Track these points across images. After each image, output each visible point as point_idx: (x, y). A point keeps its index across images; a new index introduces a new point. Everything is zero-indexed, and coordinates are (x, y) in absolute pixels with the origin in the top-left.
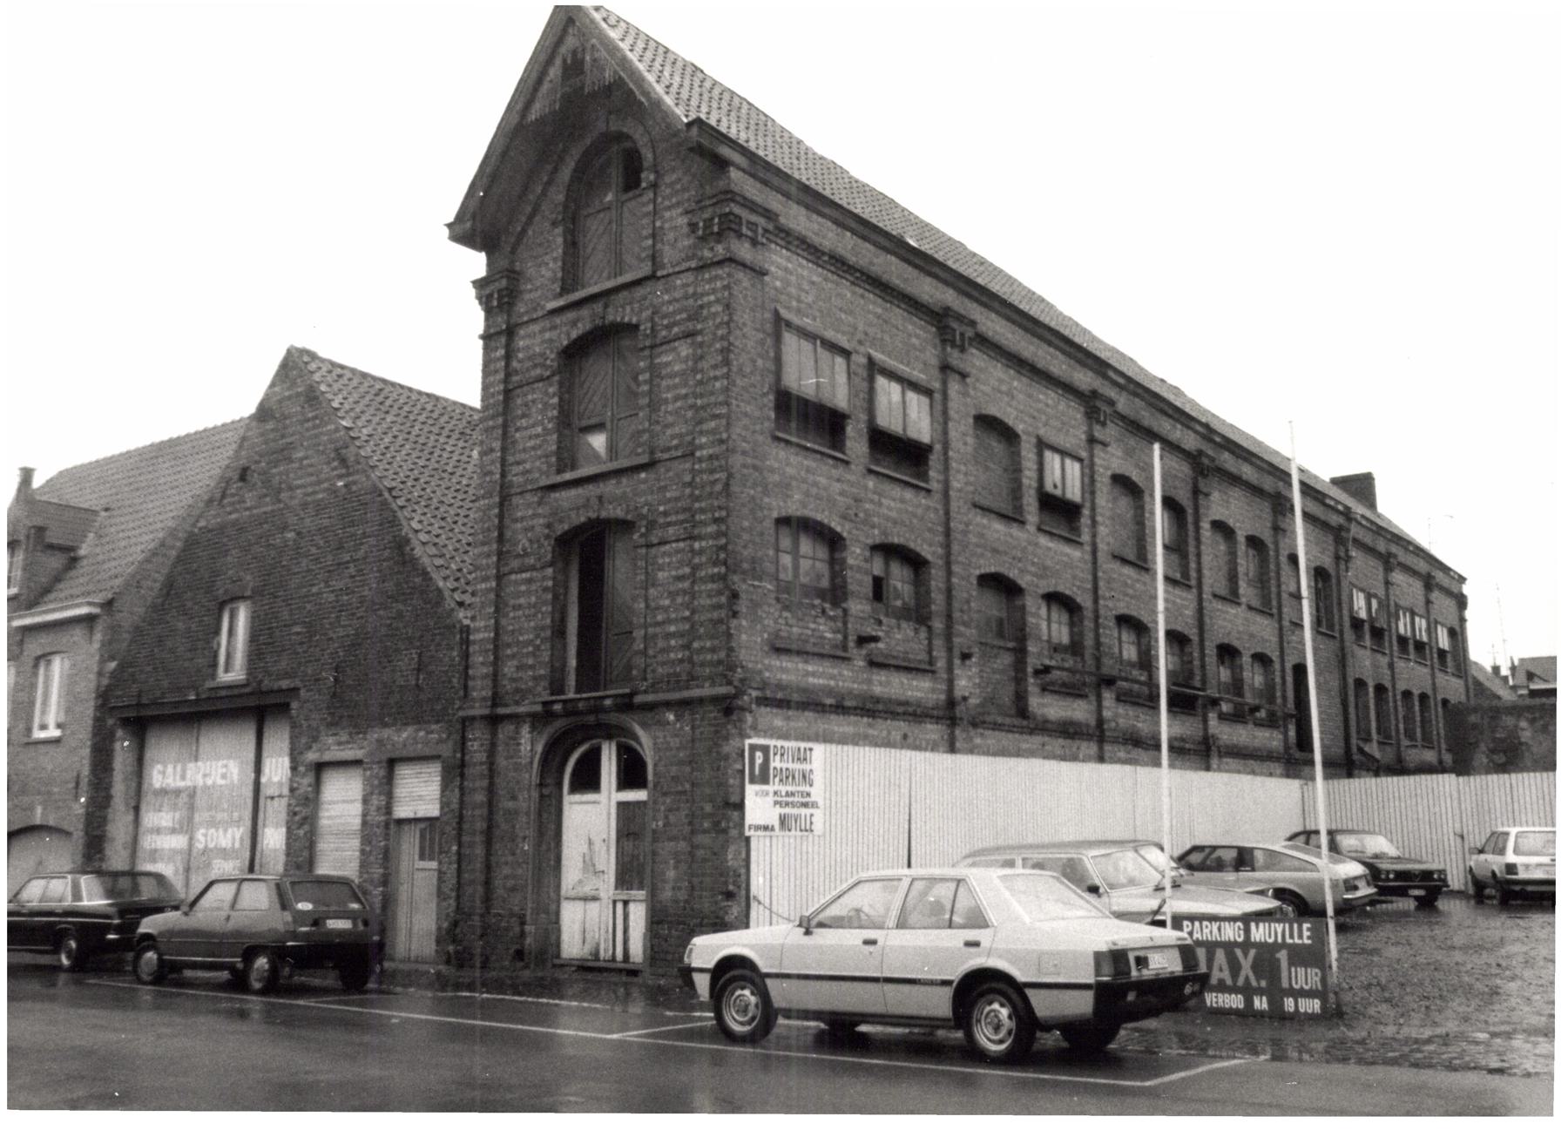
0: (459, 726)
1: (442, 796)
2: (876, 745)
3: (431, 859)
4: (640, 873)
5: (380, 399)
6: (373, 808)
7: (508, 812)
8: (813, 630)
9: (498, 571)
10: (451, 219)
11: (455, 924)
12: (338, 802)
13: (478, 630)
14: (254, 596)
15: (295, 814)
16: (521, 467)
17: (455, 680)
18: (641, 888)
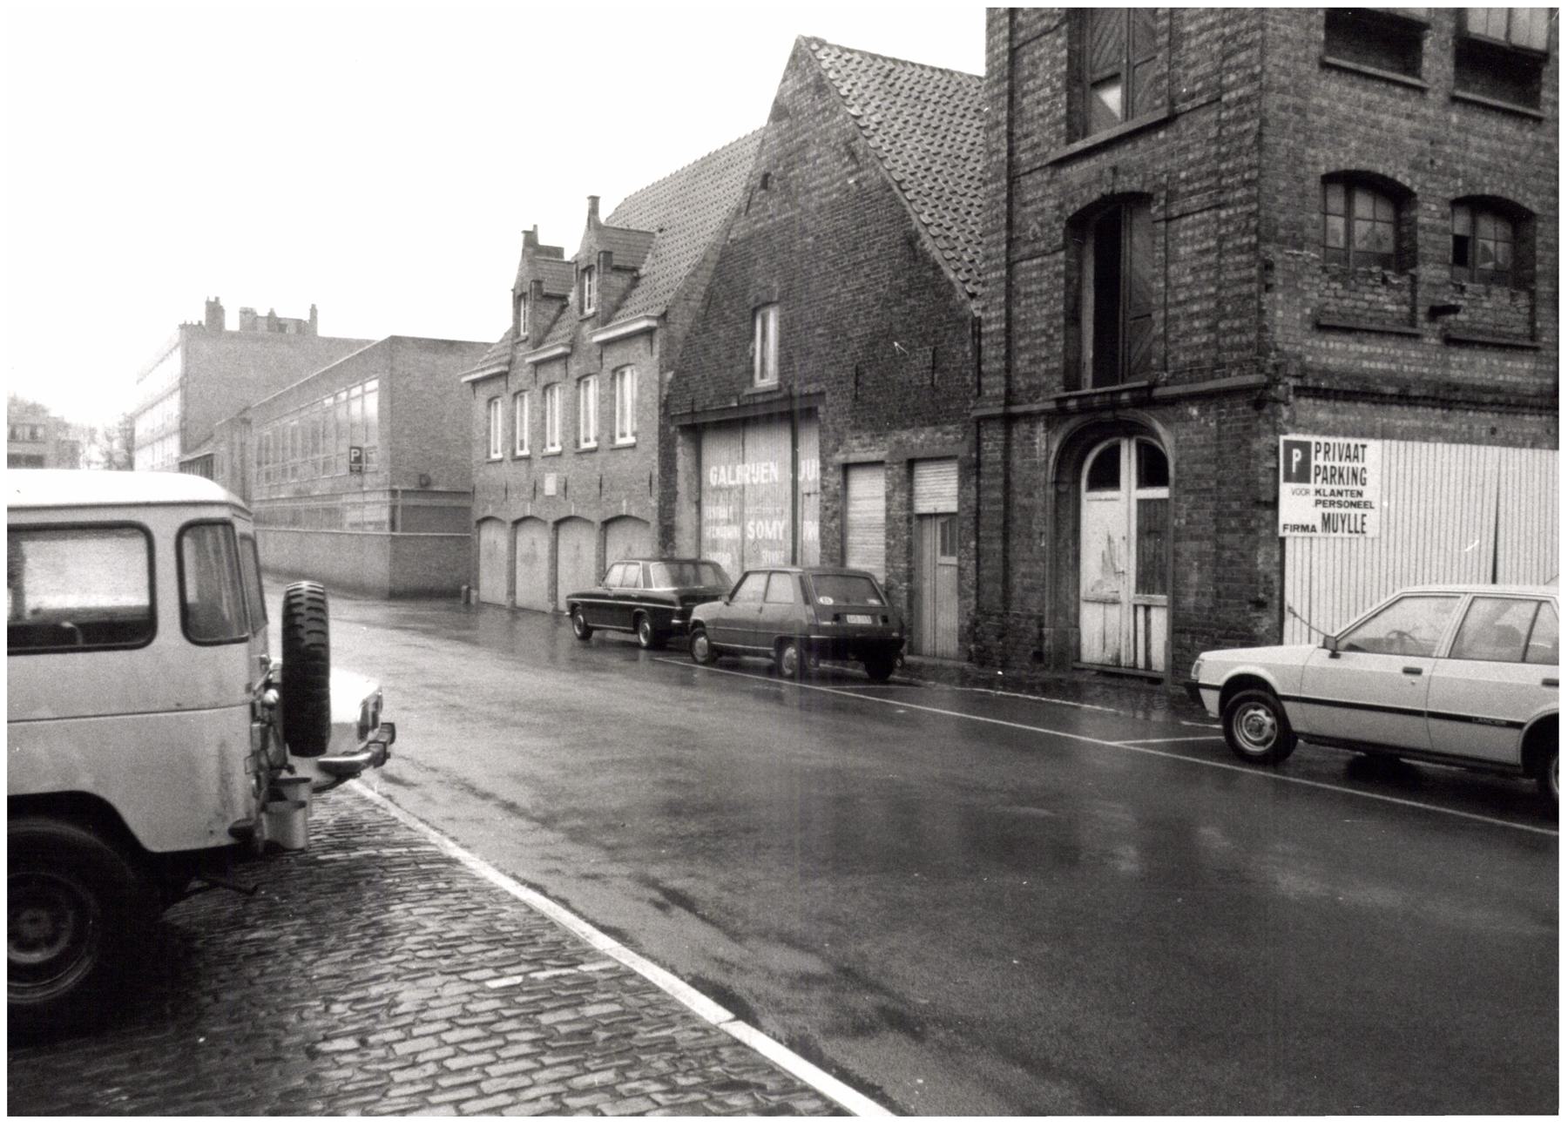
0: (974, 426)
1: (960, 492)
2: (1453, 441)
3: (952, 554)
4: (1162, 576)
5: (890, 81)
6: (896, 504)
7: (1024, 507)
8: (1371, 302)
9: (1008, 259)
11: (976, 623)
12: (864, 498)
13: (989, 321)
14: (784, 299)
15: (827, 509)
16: (1029, 141)
17: (968, 378)
18: (1163, 592)
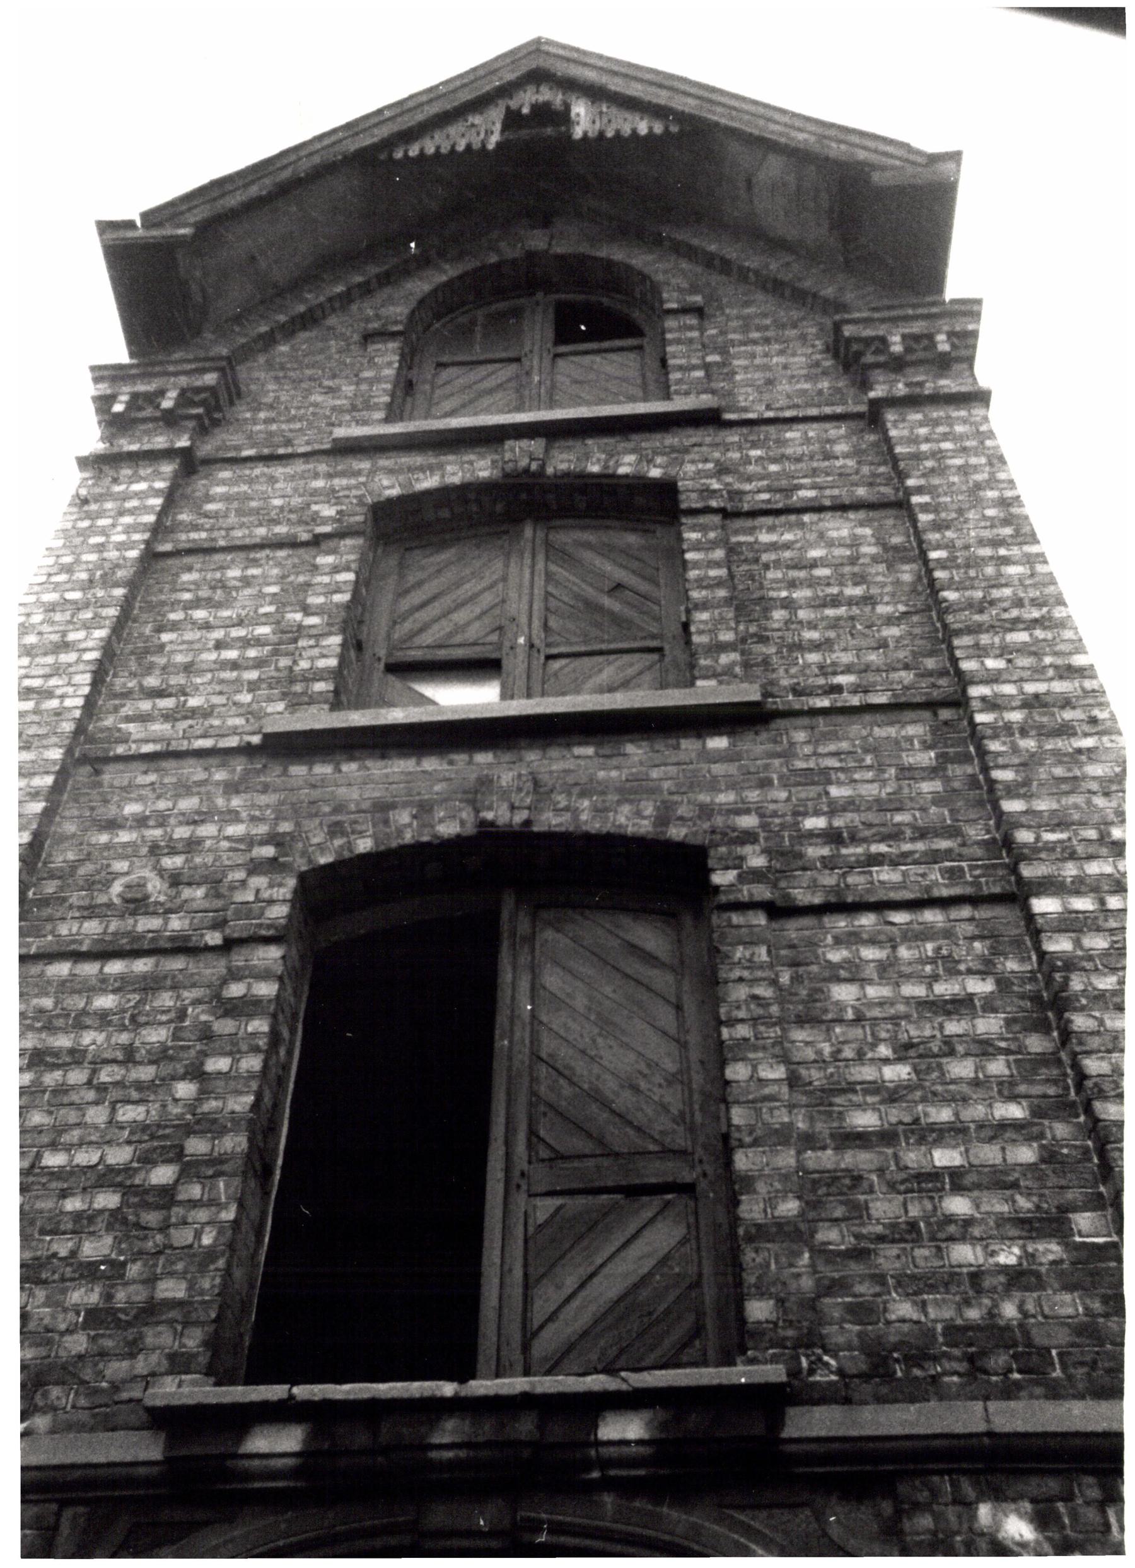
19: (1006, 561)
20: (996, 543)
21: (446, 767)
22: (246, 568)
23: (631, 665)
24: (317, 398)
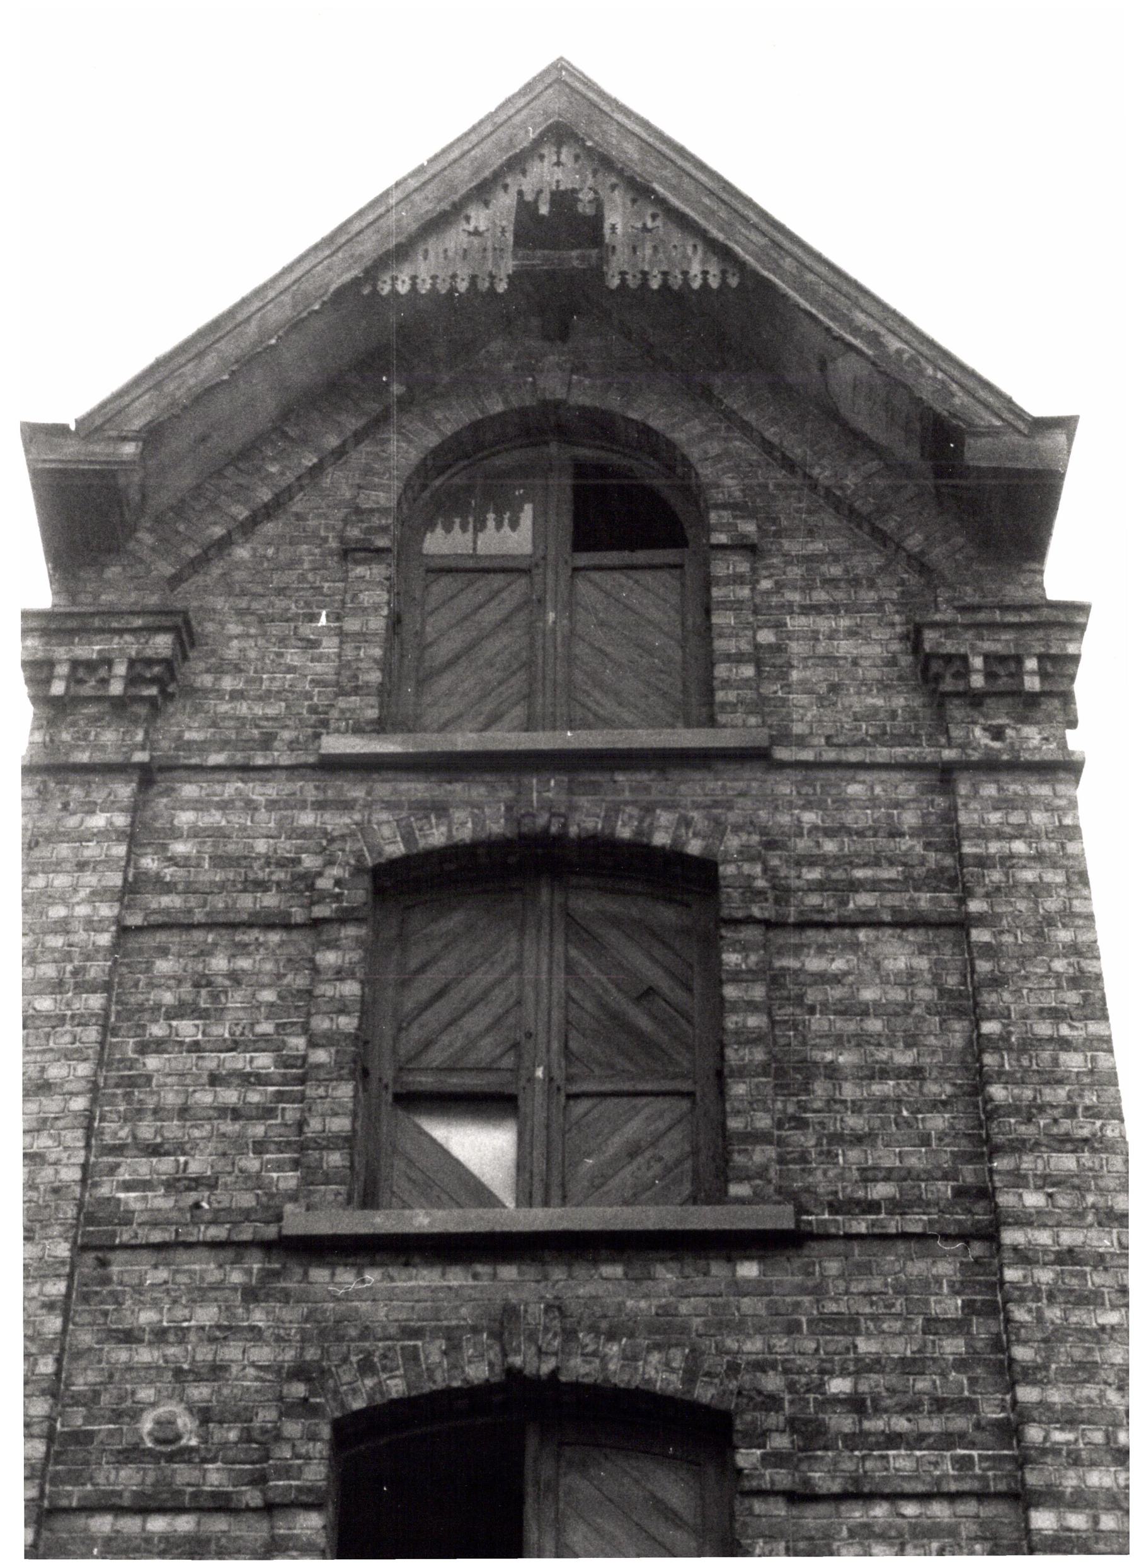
10: (69, 415)
19: (1065, 1044)
20: (1056, 1015)
21: (471, 1282)
22: (234, 956)
23: (661, 1115)
24: (293, 657)
